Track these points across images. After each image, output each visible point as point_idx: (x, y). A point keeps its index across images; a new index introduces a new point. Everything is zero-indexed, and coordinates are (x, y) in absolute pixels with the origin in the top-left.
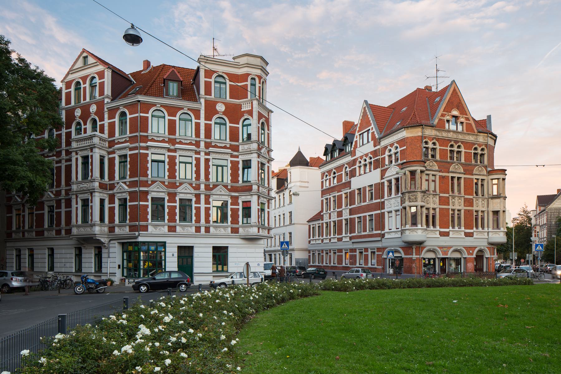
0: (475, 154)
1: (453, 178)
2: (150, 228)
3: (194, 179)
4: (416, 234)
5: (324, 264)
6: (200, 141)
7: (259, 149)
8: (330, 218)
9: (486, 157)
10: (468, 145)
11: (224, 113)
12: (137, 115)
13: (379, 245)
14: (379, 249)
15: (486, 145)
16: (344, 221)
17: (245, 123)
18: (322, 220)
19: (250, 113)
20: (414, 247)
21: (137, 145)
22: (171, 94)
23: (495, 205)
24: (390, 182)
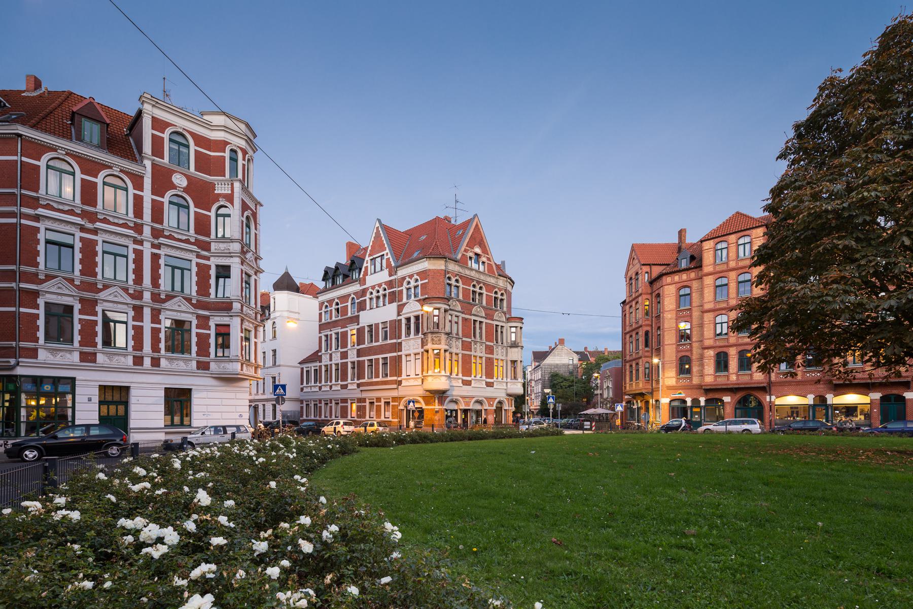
1: (475, 321)
2: (43, 355)
3: (131, 282)
5: (323, 417)
6: (142, 225)
8: (331, 360)
9: (505, 302)
10: (490, 288)
11: (186, 190)
13: (394, 394)
14: (394, 399)
15: (506, 290)
16: (350, 365)
17: (220, 212)
18: (320, 362)
19: (230, 198)
21: (14, 209)
22: (87, 139)
23: (514, 354)
24: (408, 319)
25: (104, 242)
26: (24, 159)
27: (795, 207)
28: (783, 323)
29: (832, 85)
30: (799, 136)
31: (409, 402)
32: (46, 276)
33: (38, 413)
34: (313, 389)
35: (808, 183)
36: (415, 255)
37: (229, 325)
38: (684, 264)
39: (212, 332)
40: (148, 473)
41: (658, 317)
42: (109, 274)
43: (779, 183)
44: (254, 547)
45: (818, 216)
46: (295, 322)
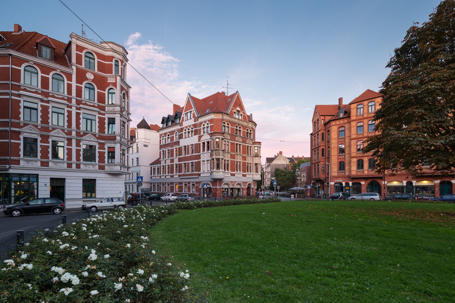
1: (237, 144)
2: (22, 163)
3: (66, 127)
4: (219, 174)
5: (162, 192)
6: (71, 98)
7: (121, 111)
9: (252, 134)
10: (244, 127)
11: (93, 81)
13: (197, 180)
14: (197, 183)
15: (252, 129)
16: (175, 166)
18: (160, 164)
19: (115, 84)
20: (218, 182)
21: (8, 91)
22: (44, 56)
23: (256, 160)
24: (204, 143)
25: (52, 107)
26: (13, 66)
27: (394, 93)
28: (388, 149)
29: (414, 30)
30: (397, 55)
31: (204, 185)
32: (24, 124)
33: (20, 192)
34: (157, 178)
35: (402, 80)
36: (207, 111)
37: (114, 148)
38: (341, 115)
39: (106, 151)
40: (70, 234)
41: (328, 142)
42: (55, 123)
43: (386, 80)
44: (115, 287)
45: (406, 97)
46: (148, 144)
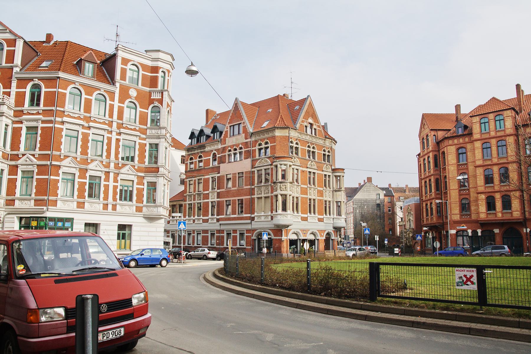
0: (324, 155)
10: (320, 147)
11: (136, 98)
12: (55, 90)
13: (249, 227)
14: (248, 231)
36: (265, 124)
